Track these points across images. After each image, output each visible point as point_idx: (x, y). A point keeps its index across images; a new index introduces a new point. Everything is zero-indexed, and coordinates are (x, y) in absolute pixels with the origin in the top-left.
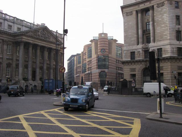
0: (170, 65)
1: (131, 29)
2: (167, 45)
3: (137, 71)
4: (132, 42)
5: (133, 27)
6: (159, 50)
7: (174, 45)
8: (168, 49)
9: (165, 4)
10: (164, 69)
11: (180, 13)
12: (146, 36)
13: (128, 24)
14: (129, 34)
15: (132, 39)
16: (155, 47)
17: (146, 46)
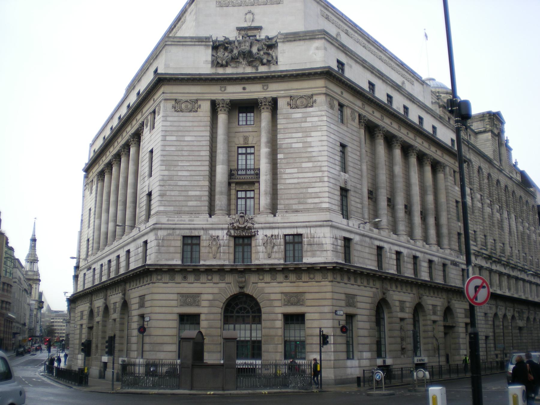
2: (320, 226)
3: (204, 303)
4: (190, 203)
5: (197, 153)
8: (324, 241)
10: (308, 303)
13: (181, 138)
14: (180, 173)
15: (191, 193)
17: (247, 221)
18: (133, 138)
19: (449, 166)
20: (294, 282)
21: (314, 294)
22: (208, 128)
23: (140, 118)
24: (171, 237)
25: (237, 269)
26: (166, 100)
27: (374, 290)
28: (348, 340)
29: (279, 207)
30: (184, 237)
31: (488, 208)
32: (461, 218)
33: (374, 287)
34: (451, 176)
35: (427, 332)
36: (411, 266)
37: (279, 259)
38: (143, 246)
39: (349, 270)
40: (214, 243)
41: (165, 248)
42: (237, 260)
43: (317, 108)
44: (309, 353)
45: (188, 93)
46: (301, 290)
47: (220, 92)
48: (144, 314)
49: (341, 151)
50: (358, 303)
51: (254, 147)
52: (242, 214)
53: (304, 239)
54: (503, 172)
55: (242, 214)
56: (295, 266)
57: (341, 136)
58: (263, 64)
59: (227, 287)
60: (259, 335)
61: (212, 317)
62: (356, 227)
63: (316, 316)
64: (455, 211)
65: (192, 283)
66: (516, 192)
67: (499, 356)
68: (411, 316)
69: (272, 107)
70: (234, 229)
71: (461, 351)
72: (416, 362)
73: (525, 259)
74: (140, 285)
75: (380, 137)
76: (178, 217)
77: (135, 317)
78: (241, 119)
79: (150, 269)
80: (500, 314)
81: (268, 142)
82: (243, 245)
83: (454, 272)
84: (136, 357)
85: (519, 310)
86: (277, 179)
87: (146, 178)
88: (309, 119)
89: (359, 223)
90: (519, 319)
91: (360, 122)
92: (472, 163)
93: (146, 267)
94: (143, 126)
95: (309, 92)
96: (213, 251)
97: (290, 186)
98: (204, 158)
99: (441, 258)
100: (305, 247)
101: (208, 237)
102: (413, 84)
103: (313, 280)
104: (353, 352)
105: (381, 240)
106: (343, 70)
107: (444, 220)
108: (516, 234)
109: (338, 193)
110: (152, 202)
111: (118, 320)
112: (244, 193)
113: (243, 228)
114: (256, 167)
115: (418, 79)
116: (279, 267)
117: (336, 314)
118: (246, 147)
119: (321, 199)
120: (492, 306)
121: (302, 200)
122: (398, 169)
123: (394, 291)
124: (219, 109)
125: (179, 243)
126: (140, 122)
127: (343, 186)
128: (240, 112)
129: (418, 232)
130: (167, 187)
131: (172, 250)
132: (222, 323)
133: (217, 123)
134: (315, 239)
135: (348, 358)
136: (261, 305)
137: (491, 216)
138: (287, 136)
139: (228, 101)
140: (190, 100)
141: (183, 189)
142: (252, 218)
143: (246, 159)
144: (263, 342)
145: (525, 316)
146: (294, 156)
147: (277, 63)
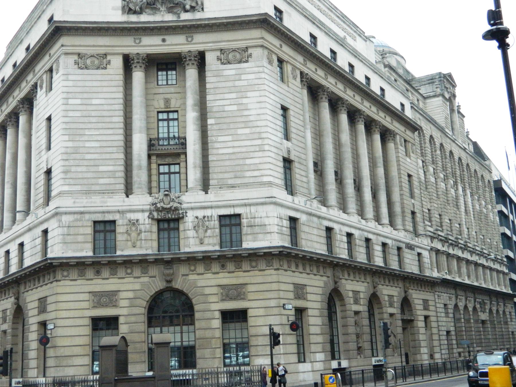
2: (262, 204)
3: (124, 303)
4: (102, 181)
5: (108, 120)
8: (266, 221)
9: (250, 56)
10: (251, 296)
14: (88, 144)
15: (101, 168)
16: (211, 207)
17: (173, 200)
18: (22, 104)
19: (400, 135)
20: (233, 272)
22: (121, 89)
23: (31, 79)
24: (80, 224)
25: (163, 259)
26: (66, 54)
27: (325, 279)
28: (299, 339)
29: (212, 182)
30: (95, 222)
31: (442, 184)
32: (110, 348)
33: (324, 275)
34: (401, 145)
35: (348, 342)
36: (363, 250)
37: (214, 245)
38: (42, 236)
39: (297, 255)
40: (134, 228)
41: (72, 237)
42: (161, 248)
43: (253, 63)
44: (253, 357)
45: (94, 46)
47: (134, 44)
48: (46, 321)
49: (282, 115)
51: (177, 111)
52: (166, 193)
53: (242, 220)
54: (456, 142)
55: (166, 193)
56: (233, 253)
57: (282, 96)
58: (186, 11)
59: (150, 281)
60: (192, 338)
61: (133, 319)
62: (302, 204)
63: (261, 312)
64: (407, 186)
65: (107, 279)
66: (470, 165)
67: (462, 354)
68: (366, 308)
69: (199, 62)
70: (158, 210)
71: (422, 349)
72: (374, 363)
73: (484, 242)
74: (39, 285)
76: (87, 198)
77: (34, 325)
78: (160, 78)
79: (54, 264)
80: (461, 305)
81: (195, 105)
82: (169, 229)
83: (410, 256)
84: (36, 376)
85: (481, 300)
86: (208, 150)
87: (44, 152)
88: (243, 77)
89: (305, 199)
90: (481, 311)
91: (302, 81)
92: (423, 131)
93: (49, 261)
94: (36, 89)
95: (242, 44)
96: (132, 239)
97: (224, 157)
98: (117, 125)
99: (395, 240)
100: (245, 230)
101: (126, 222)
102: (355, 40)
103: (256, 269)
104: (304, 353)
105: (330, 220)
106: (281, 19)
107: (396, 197)
108: (472, 213)
109: (281, 164)
110: (53, 181)
111: (9, 331)
112: (166, 167)
113: (169, 209)
114: (182, 135)
115: (361, 34)
117: (284, 309)
118: (168, 112)
119: (261, 171)
120: (451, 296)
121: (239, 174)
122: (345, 137)
123: (346, 280)
124: (133, 66)
125: (89, 230)
126: (32, 83)
127: (286, 156)
128: (159, 70)
129: (370, 212)
130: (72, 161)
131: (80, 238)
132: (146, 326)
133: (131, 83)
134: (256, 220)
135: (299, 362)
136: (194, 301)
137: (447, 192)
138: (218, 97)
139: (145, 55)
140: (97, 55)
141: (92, 163)
142: (179, 197)
143: (168, 127)
144: (197, 347)
145: (487, 307)
146: (227, 120)
147: (203, 9)
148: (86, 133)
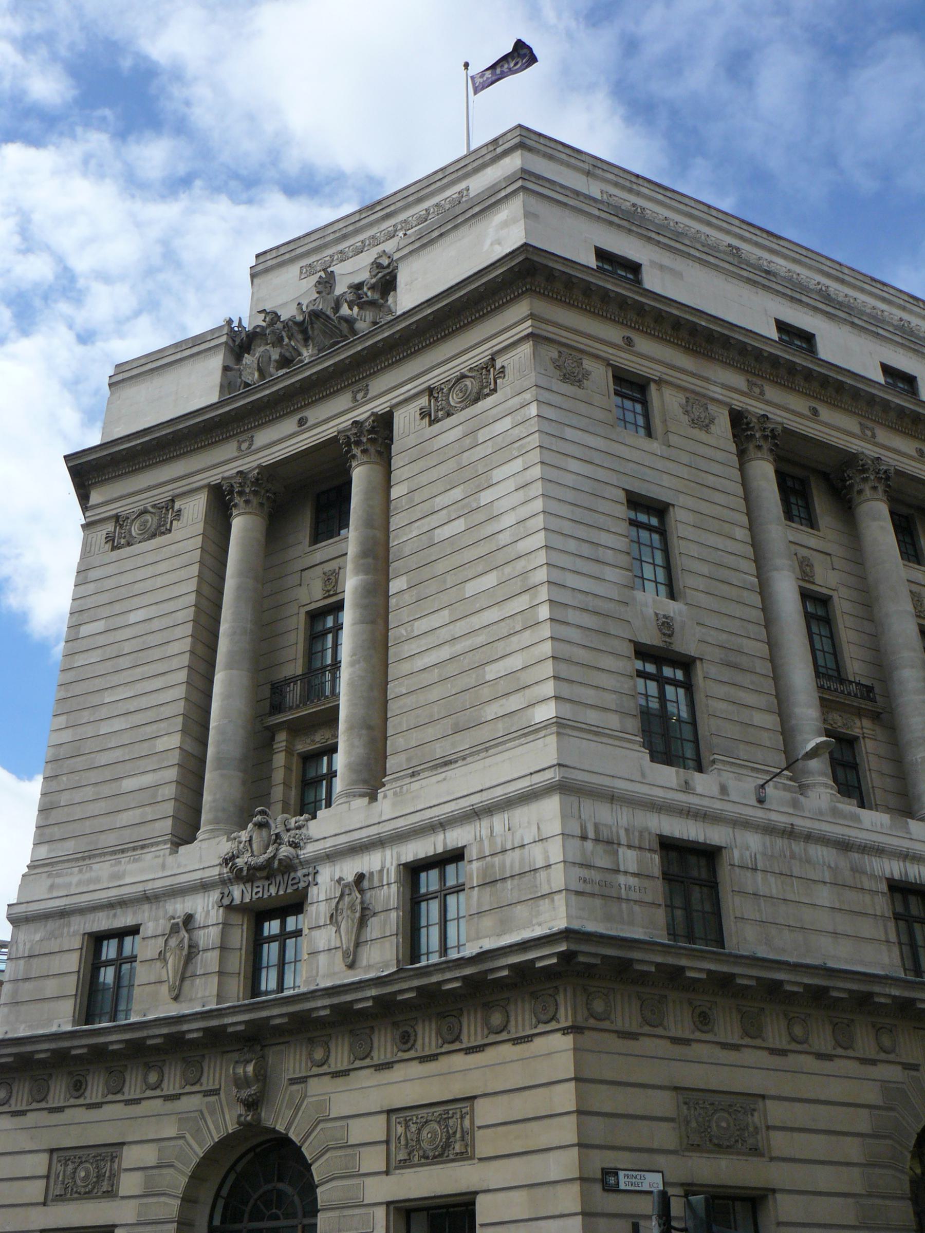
0: (571, 1137)
1: (138, 672)
3: (129, 1184)
5: (157, 654)
6: (430, 881)
7: (612, 798)
8: (537, 856)
10: (484, 1145)
11: (666, 481)
12: (289, 751)
14: (105, 728)
15: (128, 784)
21: (505, 1097)
46: (457, 1089)
50: (772, 1134)
75: (868, 493)
88: (482, 436)
101: (163, 925)
116: (360, 995)
134: (509, 857)
138: (418, 512)
140: (154, 506)
148: (107, 700)
